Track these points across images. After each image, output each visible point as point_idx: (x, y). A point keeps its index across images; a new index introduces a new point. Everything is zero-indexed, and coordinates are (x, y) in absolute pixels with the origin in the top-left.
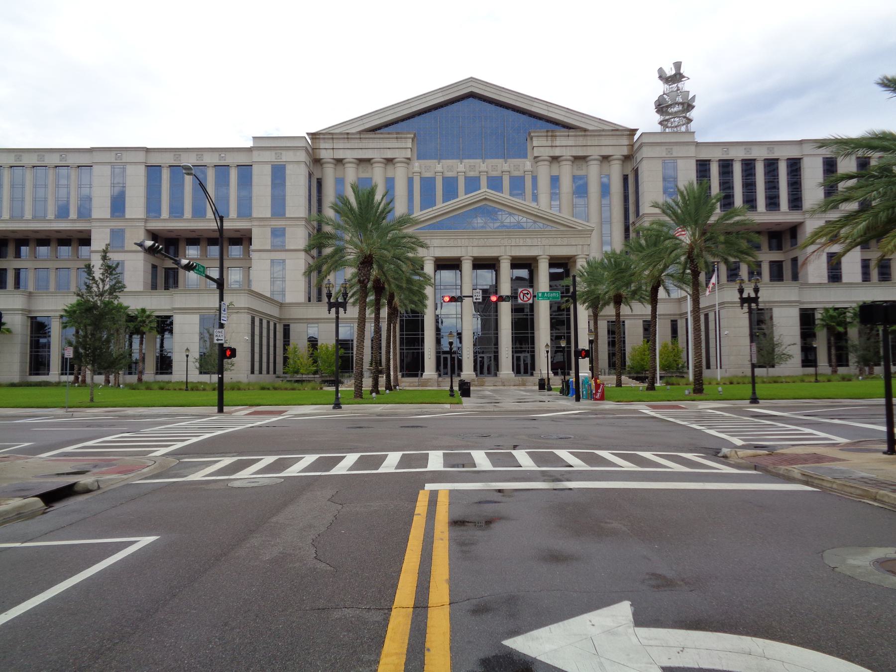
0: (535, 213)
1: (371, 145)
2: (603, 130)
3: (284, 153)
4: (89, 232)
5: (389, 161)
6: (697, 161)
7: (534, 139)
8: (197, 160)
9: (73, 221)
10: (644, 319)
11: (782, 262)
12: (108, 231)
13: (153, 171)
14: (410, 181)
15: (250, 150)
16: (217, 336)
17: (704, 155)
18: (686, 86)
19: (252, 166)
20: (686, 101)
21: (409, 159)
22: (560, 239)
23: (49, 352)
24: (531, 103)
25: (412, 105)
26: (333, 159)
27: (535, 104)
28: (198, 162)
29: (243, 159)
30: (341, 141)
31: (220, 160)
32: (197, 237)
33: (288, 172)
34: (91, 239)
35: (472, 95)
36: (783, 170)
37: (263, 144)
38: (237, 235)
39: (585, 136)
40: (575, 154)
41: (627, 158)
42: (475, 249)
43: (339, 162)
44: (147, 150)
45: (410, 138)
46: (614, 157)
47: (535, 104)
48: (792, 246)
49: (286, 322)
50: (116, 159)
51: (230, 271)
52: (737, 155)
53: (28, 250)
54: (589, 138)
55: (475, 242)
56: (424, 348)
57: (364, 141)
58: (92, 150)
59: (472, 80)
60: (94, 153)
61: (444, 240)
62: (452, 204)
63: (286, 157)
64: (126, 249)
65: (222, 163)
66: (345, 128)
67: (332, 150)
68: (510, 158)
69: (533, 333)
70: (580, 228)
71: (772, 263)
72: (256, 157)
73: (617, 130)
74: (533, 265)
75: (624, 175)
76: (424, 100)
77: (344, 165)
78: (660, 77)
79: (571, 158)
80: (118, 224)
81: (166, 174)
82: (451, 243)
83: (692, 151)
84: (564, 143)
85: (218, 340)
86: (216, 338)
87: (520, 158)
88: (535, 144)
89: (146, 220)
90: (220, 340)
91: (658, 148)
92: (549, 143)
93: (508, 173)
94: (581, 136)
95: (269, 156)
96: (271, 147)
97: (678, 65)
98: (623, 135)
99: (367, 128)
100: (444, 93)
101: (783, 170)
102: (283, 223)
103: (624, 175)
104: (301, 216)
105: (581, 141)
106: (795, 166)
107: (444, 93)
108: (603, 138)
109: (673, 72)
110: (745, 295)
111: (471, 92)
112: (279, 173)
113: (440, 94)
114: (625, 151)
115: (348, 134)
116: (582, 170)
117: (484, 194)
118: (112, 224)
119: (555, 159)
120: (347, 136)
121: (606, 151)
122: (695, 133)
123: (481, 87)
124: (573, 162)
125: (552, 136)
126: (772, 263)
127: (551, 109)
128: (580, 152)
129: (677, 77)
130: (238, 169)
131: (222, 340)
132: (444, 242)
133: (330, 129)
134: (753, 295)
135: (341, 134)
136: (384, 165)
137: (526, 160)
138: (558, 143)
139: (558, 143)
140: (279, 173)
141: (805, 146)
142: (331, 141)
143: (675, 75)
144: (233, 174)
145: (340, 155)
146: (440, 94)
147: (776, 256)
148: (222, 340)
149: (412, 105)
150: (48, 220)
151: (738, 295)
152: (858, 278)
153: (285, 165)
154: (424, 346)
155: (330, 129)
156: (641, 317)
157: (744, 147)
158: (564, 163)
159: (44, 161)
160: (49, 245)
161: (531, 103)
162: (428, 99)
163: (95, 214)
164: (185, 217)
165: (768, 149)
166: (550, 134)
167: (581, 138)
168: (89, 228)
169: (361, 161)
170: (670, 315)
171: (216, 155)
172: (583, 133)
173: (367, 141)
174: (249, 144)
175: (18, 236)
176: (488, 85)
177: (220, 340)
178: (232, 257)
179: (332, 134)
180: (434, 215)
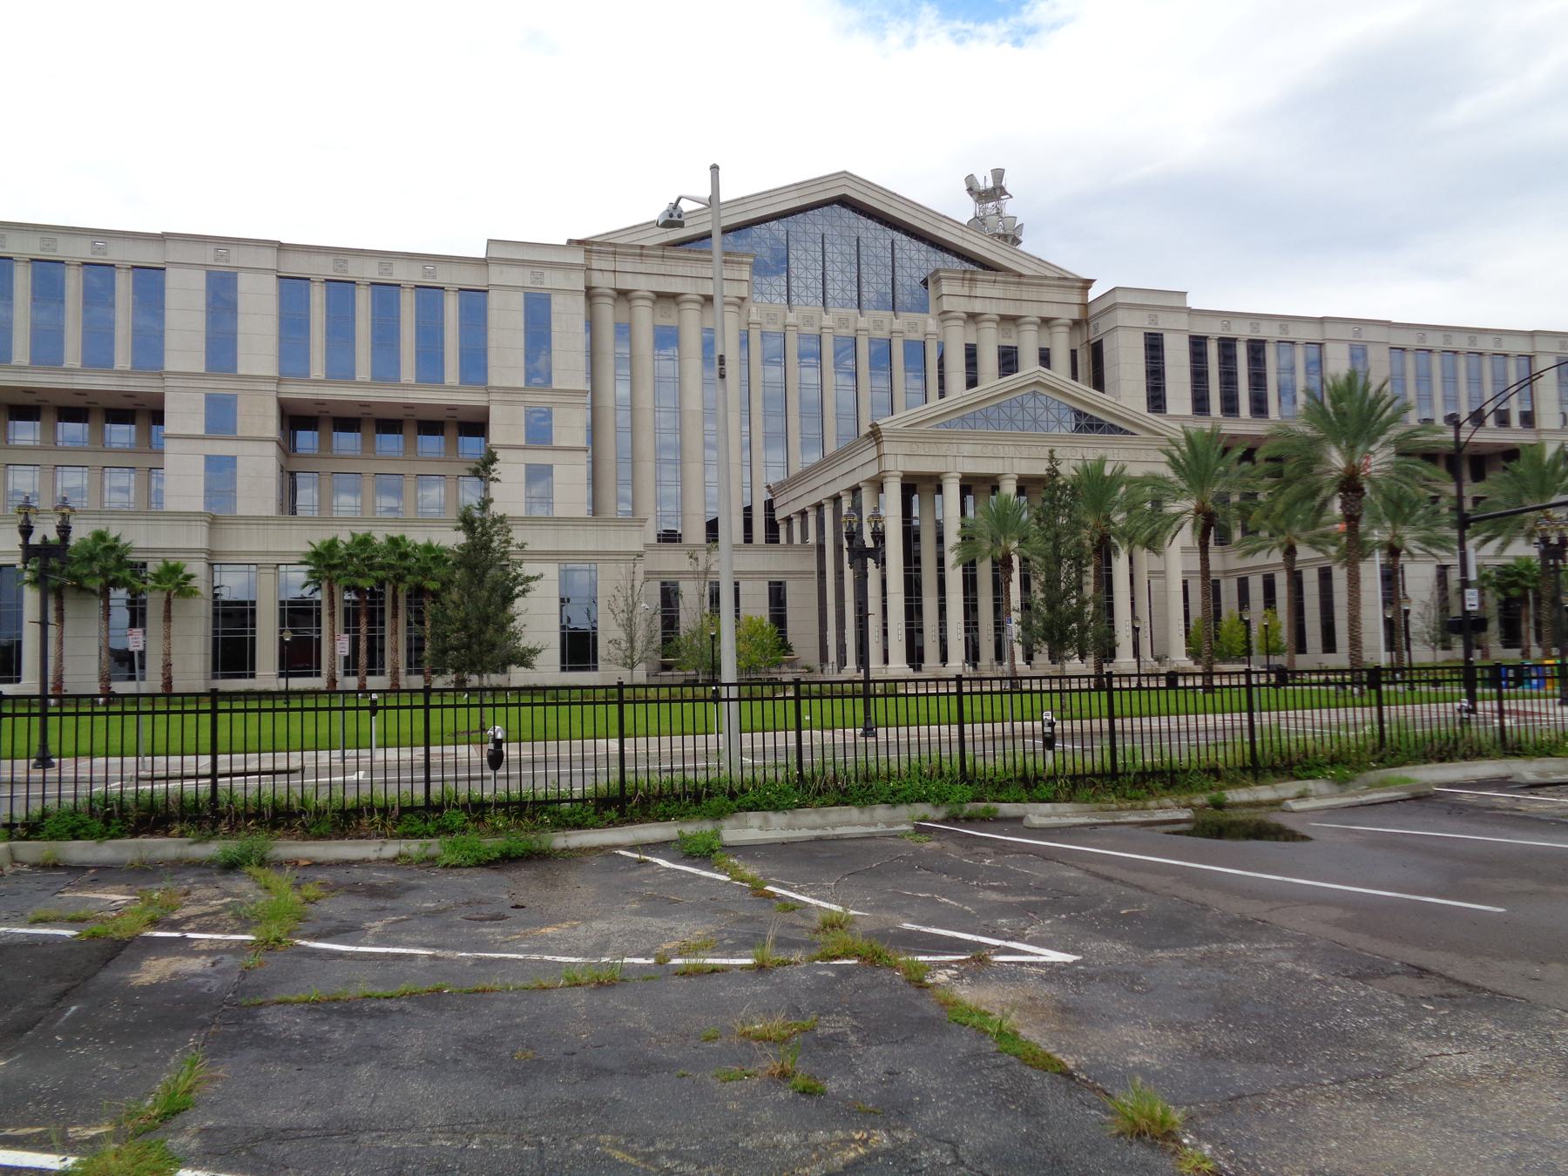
1: (680, 271)
2: (1046, 277)
3: (547, 273)
4: (160, 398)
5: (1046, 322)
6: (1190, 337)
7: (944, 282)
8: (381, 274)
9: (123, 374)
12: (202, 396)
13: (292, 287)
15: (484, 262)
17: (1200, 329)
18: (1009, 207)
19: (164, 269)
21: (743, 299)
23: (253, 632)
24: (937, 224)
25: (749, 207)
26: (615, 289)
27: (943, 226)
29: (471, 279)
30: (630, 259)
31: (424, 276)
32: (35, 403)
33: (555, 308)
34: (163, 412)
35: (844, 202)
37: (503, 254)
39: (1019, 283)
40: (1002, 312)
41: (1077, 324)
42: (1024, 462)
43: (623, 295)
44: (280, 247)
47: (943, 226)
50: (216, 260)
51: (59, 474)
52: (1242, 331)
53: (87, 429)
54: (1024, 288)
55: (1025, 452)
57: (668, 262)
58: (164, 238)
59: (845, 175)
60: (169, 245)
61: (979, 447)
63: (552, 280)
64: (239, 433)
65: (429, 282)
66: (634, 237)
67: (612, 275)
69: (976, 600)
72: (496, 276)
73: (1066, 279)
75: (1041, 350)
76: (769, 201)
77: (629, 301)
78: (970, 190)
79: (651, 295)
80: (223, 386)
81: (318, 296)
82: (989, 451)
83: (1182, 322)
84: (988, 293)
88: (945, 290)
89: (280, 381)
91: (1138, 314)
92: (966, 291)
94: (1013, 283)
96: (524, 261)
97: (998, 174)
98: (1072, 287)
100: (801, 193)
102: (547, 398)
103: (1041, 350)
104: (271, 374)
105: (1013, 292)
107: (801, 193)
108: (1044, 289)
109: (990, 184)
110: (35, 540)
111: (845, 196)
112: (538, 311)
113: (795, 194)
114: (1075, 313)
115: (642, 247)
118: (210, 384)
119: (973, 317)
120: (641, 252)
121: (1048, 311)
122: (1094, 284)
123: (859, 188)
124: (654, 302)
125: (971, 280)
128: (1011, 310)
129: (996, 192)
130: (373, 291)
132: (978, 450)
134: (53, 536)
138: (979, 292)
139: (979, 292)
140: (538, 311)
141: (1327, 326)
142: (611, 258)
143: (994, 189)
144: (123, 284)
145: (626, 283)
146: (795, 194)
149: (749, 207)
150: (65, 370)
151: (20, 540)
152: (270, 507)
153: (236, 274)
157: (1249, 321)
158: (688, 306)
159: (55, 250)
160: (86, 421)
161: (937, 224)
163: (172, 363)
164: (65, 366)
165: (1281, 326)
166: (968, 276)
167: (1013, 288)
168: (160, 391)
169: (661, 297)
171: (1276, 325)
172: (1017, 280)
173: (673, 262)
175: (422, 416)
178: (17, 443)
179: (615, 245)
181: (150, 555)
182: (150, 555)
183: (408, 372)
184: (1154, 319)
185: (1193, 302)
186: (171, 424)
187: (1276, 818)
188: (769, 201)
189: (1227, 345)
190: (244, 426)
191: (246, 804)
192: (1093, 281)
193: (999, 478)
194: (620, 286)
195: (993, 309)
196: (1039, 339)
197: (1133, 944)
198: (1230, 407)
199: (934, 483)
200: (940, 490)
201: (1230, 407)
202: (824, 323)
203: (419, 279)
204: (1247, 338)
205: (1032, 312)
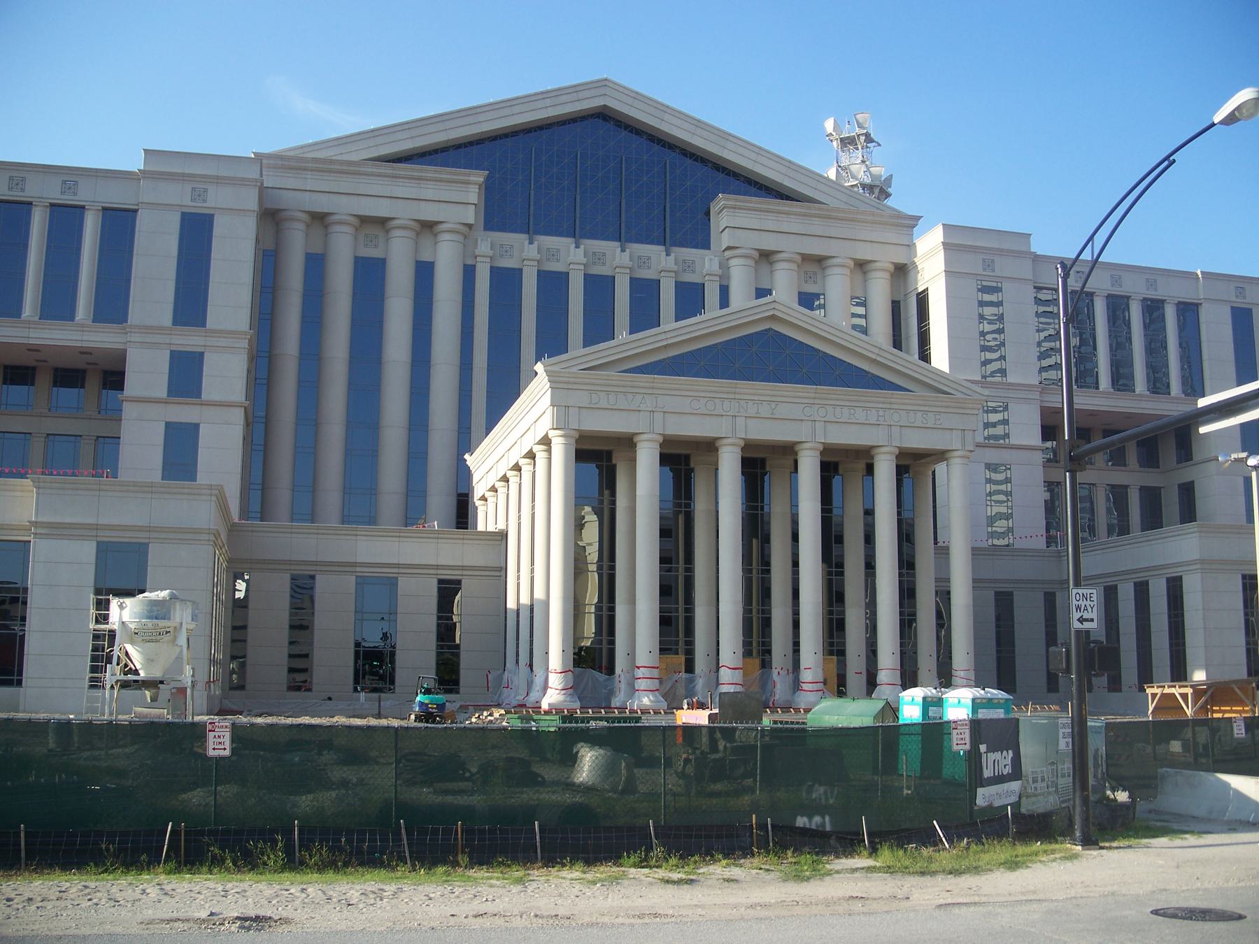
0: (874, 356)
3: (212, 189)
4: (121, 357)
5: (428, 227)
10: (997, 590)
11: (1159, 488)
14: (469, 273)
16: (1078, 608)
19: (136, 211)
20: (877, 183)
21: (470, 226)
22: (920, 413)
28: (11, 193)
29: (118, 197)
35: (604, 116)
36: (1136, 315)
38: (27, 360)
45: (475, 184)
46: (337, 217)
48: (1179, 462)
49: (1173, 572)
52: (1172, 293)
56: (770, 642)
59: (604, 83)
62: (695, 326)
63: (216, 199)
65: (68, 199)
68: (676, 246)
70: (959, 395)
71: (1144, 490)
72: (147, 193)
74: (768, 463)
76: (506, 112)
79: (352, 219)
80: (189, 340)
85: (1081, 620)
86: (1076, 615)
87: (696, 247)
90: (1087, 620)
93: (673, 274)
95: (181, 197)
99: (383, 156)
101: (1136, 315)
106: (1188, 312)
116: (376, 246)
117: (772, 306)
126: (1144, 490)
127: (760, 159)
131: (1092, 620)
133: (306, 150)
135: (315, 160)
136: (463, 238)
137: (707, 251)
147: (1151, 478)
148: (1092, 620)
149: (481, 118)
154: (770, 637)
155: (306, 150)
156: (288, 567)
159: (205, 201)
162: (516, 109)
169: (806, 258)
170: (1043, 582)
174: (135, 163)
176: (445, 118)
177: (1087, 620)
180: (665, 343)
181: (1016, 585)
182: (1016, 585)
183: (1140, 384)
184: (198, 195)
185: (1037, 247)
186: (133, 384)
187: (1149, 845)
188: (506, 112)
189: (1153, 308)
190: (211, 389)
191: (994, 839)
192: (919, 218)
193: (797, 448)
194: (860, 256)
195: (790, 247)
196: (416, 250)
197: (24, 937)
198: (1121, 379)
199: (864, 459)
200: (870, 469)
201: (1121, 379)
202: (525, 255)
203: (57, 196)
204: (1176, 301)
205: (403, 213)
